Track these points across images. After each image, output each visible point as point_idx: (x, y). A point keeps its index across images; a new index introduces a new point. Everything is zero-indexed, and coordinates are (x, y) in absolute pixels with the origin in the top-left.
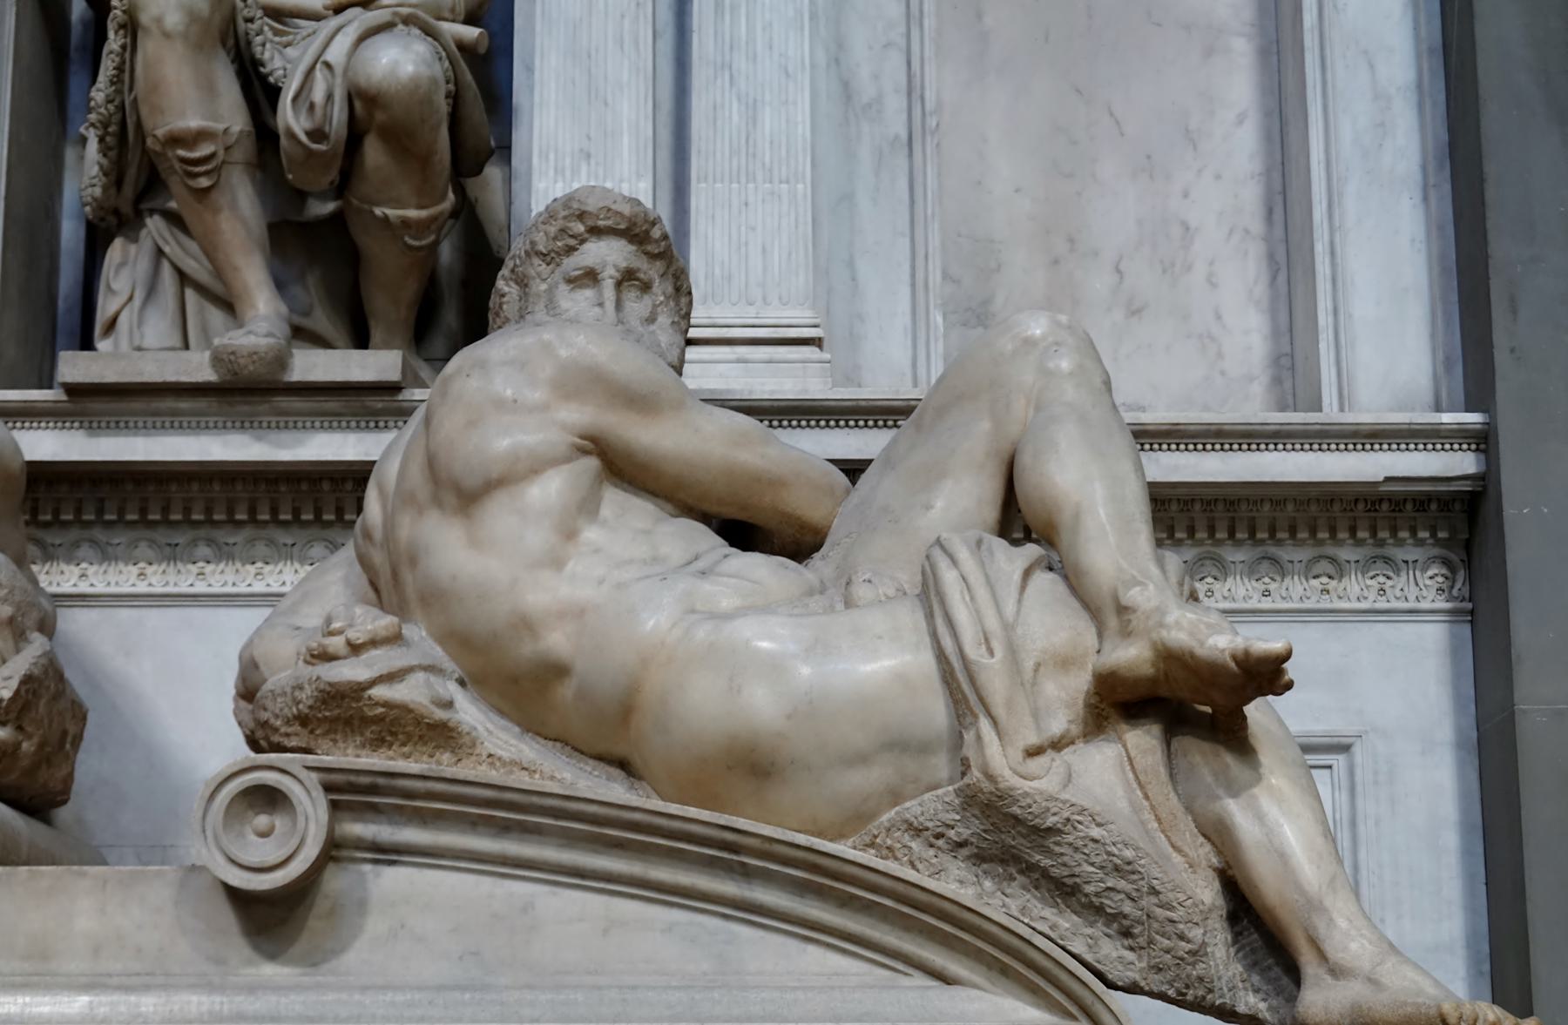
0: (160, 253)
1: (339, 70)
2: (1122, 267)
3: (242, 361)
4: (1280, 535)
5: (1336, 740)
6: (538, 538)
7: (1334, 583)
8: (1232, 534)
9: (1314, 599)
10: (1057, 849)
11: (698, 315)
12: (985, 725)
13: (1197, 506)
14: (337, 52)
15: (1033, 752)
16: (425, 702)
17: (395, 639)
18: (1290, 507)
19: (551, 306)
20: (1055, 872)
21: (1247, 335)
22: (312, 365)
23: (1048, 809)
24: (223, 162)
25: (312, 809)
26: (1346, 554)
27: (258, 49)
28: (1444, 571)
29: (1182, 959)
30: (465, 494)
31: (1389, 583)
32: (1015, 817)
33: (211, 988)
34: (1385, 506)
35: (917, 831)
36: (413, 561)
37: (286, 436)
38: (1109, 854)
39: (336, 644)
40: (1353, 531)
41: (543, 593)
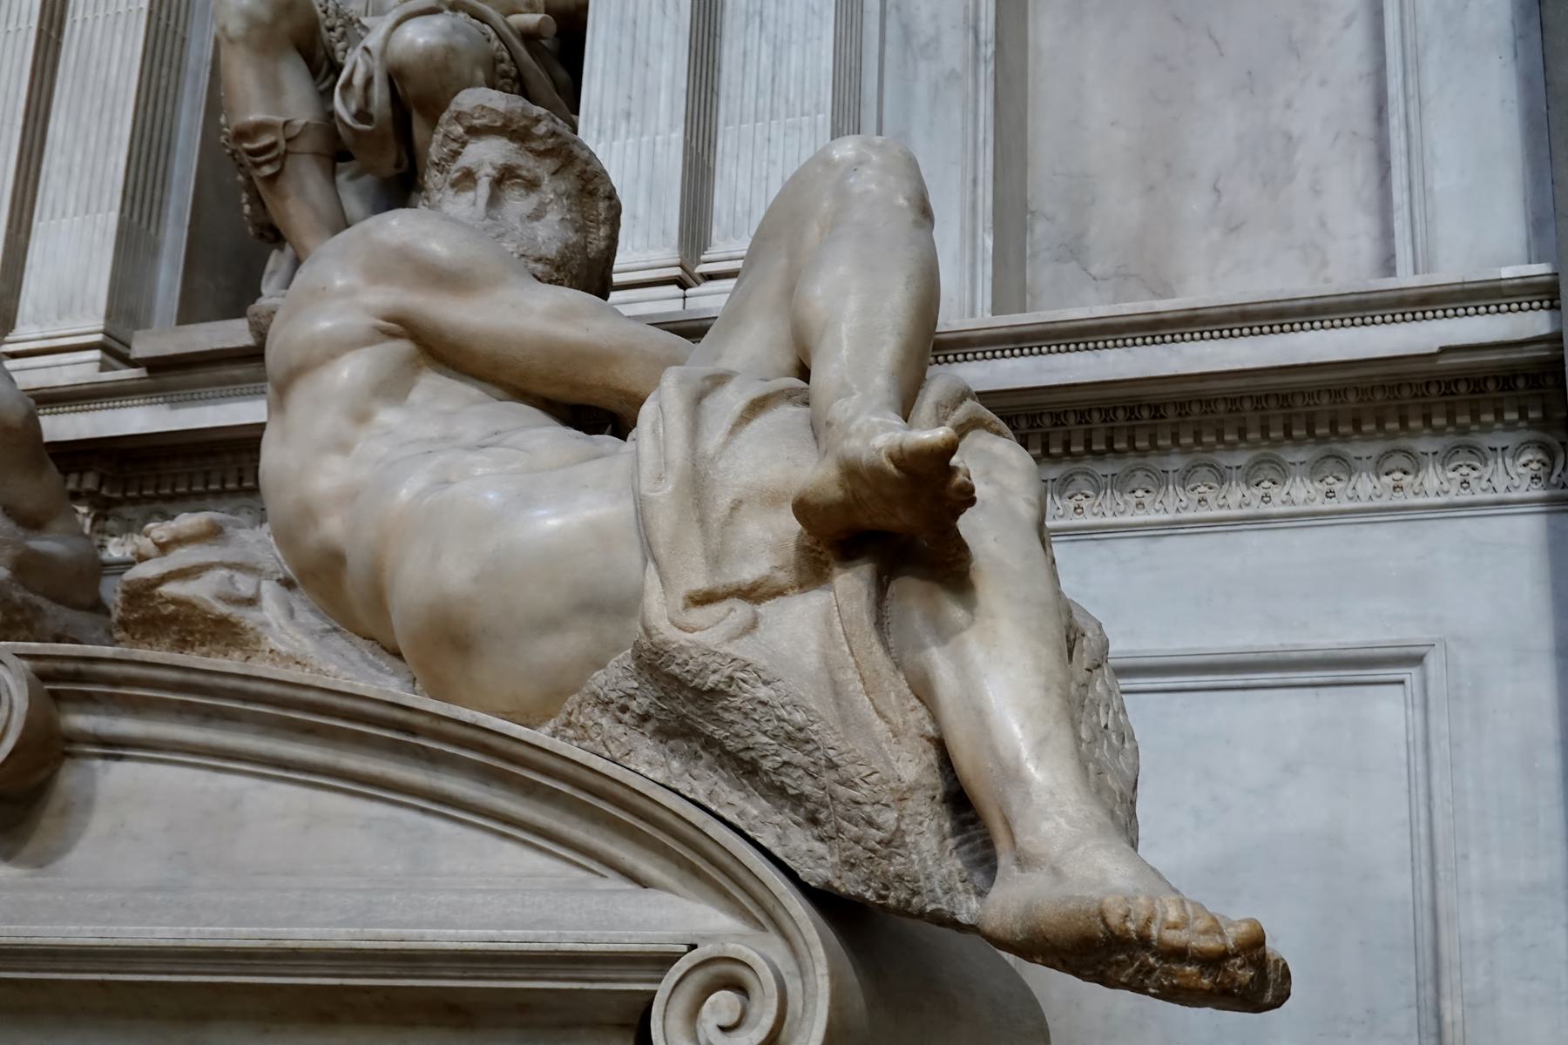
1: (376, 53)
2: (1220, 185)
4: (1343, 429)
5: (1404, 651)
7: (1409, 478)
8: (1288, 435)
9: (1385, 497)
10: (727, 716)
13: (1247, 405)
16: (206, 596)
18: (1352, 397)
20: (731, 745)
21: (1366, 248)
23: (706, 666)
24: (286, 152)
26: (1423, 445)
27: (339, 55)
28: (1540, 456)
29: (874, 851)
31: (1475, 474)
32: (675, 678)
34: (1463, 388)
35: (605, 704)
38: (780, 719)
40: (1427, 419)
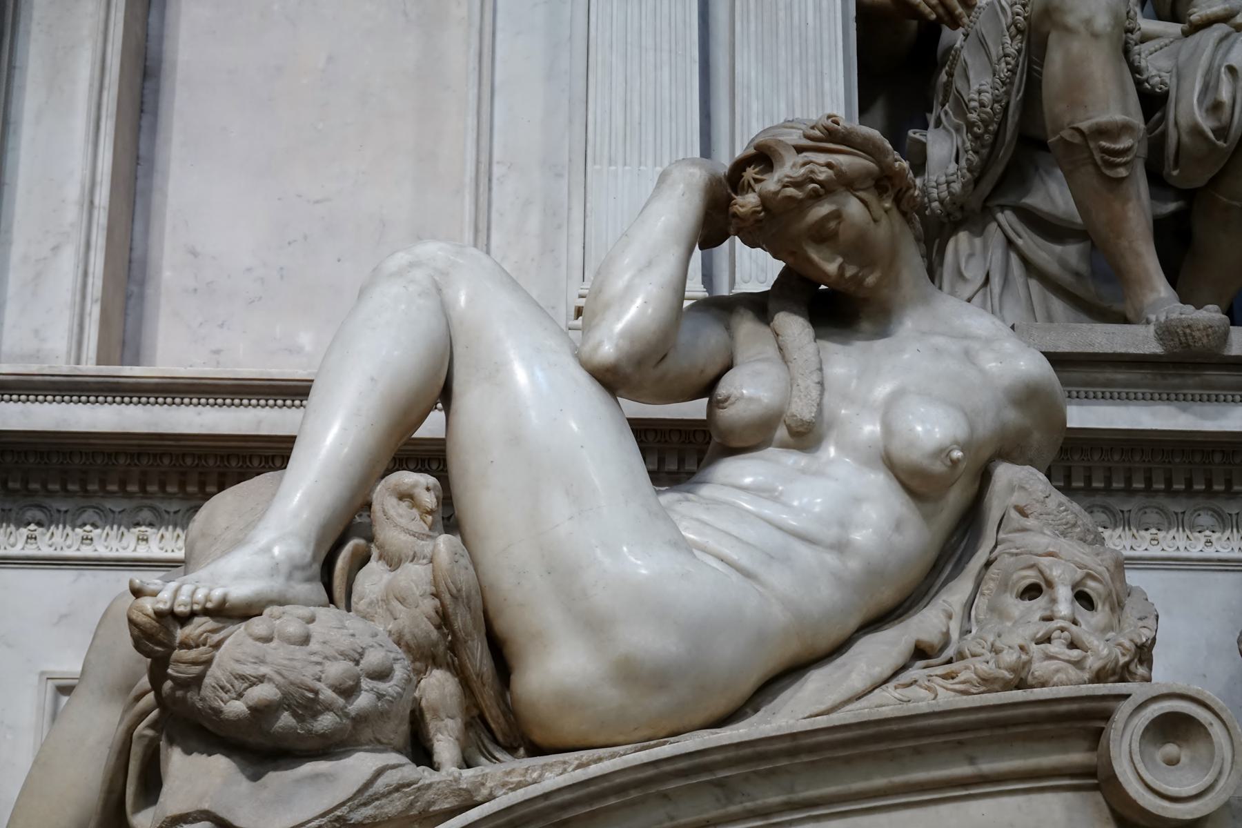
0: (1010, 243)
3: (1197, 334)
37: (1209, 408)
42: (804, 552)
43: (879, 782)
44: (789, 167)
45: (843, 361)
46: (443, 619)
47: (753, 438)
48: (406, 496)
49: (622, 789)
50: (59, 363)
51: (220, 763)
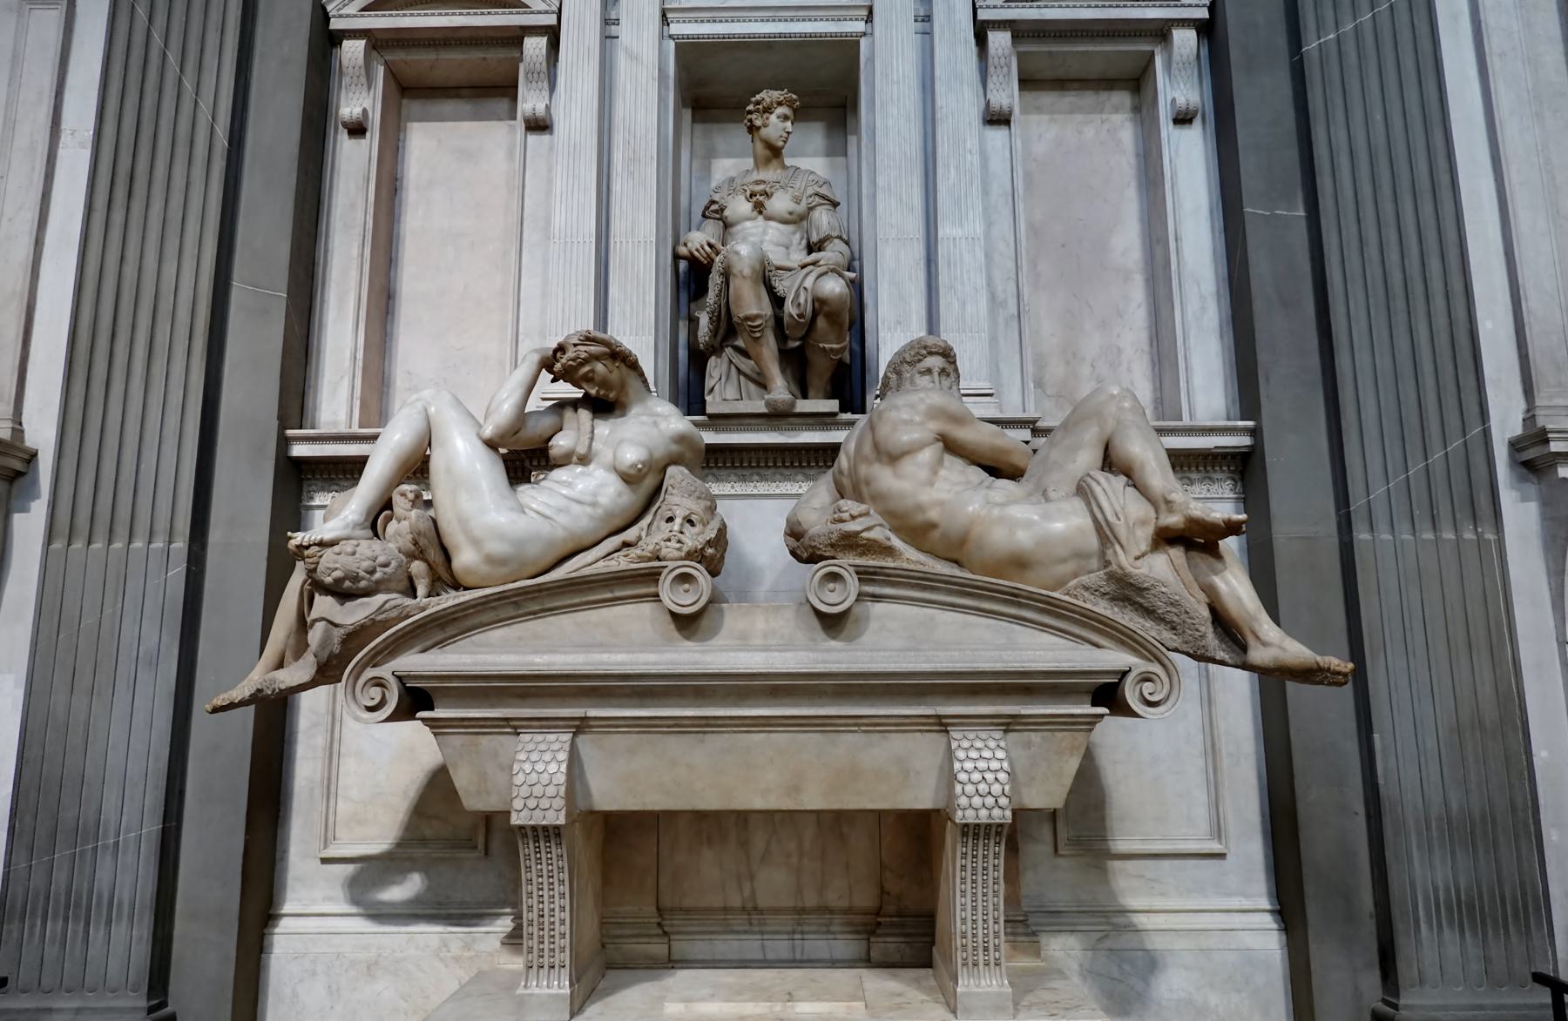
6: (924, 474)
11: (963, 384)
12: (1117, 547)
14: (808, 283)
15: (1137, 558)
17: (867, 514)
19: (912, 382)
22: (804, 406)
25: (853, 584)
26: (1194, 476)
30: (893, 458)
33: (811, 650)
35: (1086, 588)
36: (868, 483)
39: (846, 516)
41: (926, 496)
42: (576, 508)
43: (577, 601)
44: (570, 354)
45: (604, 428)
46: (416, 543)
47: (565, 461)
48: (403, 495)
49: (474, 606)
50: (343, 429)
51: (329, 599)
